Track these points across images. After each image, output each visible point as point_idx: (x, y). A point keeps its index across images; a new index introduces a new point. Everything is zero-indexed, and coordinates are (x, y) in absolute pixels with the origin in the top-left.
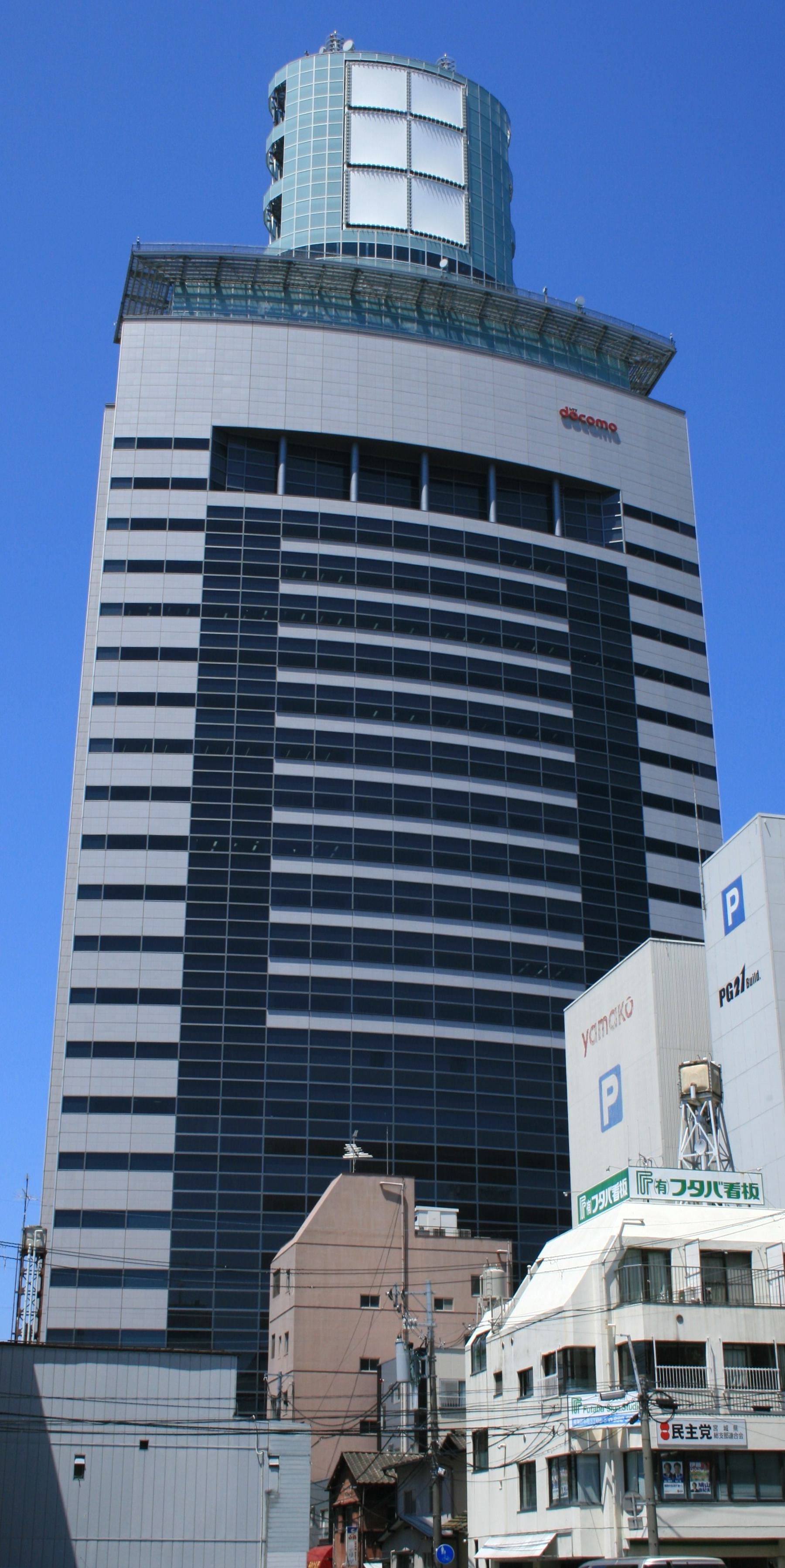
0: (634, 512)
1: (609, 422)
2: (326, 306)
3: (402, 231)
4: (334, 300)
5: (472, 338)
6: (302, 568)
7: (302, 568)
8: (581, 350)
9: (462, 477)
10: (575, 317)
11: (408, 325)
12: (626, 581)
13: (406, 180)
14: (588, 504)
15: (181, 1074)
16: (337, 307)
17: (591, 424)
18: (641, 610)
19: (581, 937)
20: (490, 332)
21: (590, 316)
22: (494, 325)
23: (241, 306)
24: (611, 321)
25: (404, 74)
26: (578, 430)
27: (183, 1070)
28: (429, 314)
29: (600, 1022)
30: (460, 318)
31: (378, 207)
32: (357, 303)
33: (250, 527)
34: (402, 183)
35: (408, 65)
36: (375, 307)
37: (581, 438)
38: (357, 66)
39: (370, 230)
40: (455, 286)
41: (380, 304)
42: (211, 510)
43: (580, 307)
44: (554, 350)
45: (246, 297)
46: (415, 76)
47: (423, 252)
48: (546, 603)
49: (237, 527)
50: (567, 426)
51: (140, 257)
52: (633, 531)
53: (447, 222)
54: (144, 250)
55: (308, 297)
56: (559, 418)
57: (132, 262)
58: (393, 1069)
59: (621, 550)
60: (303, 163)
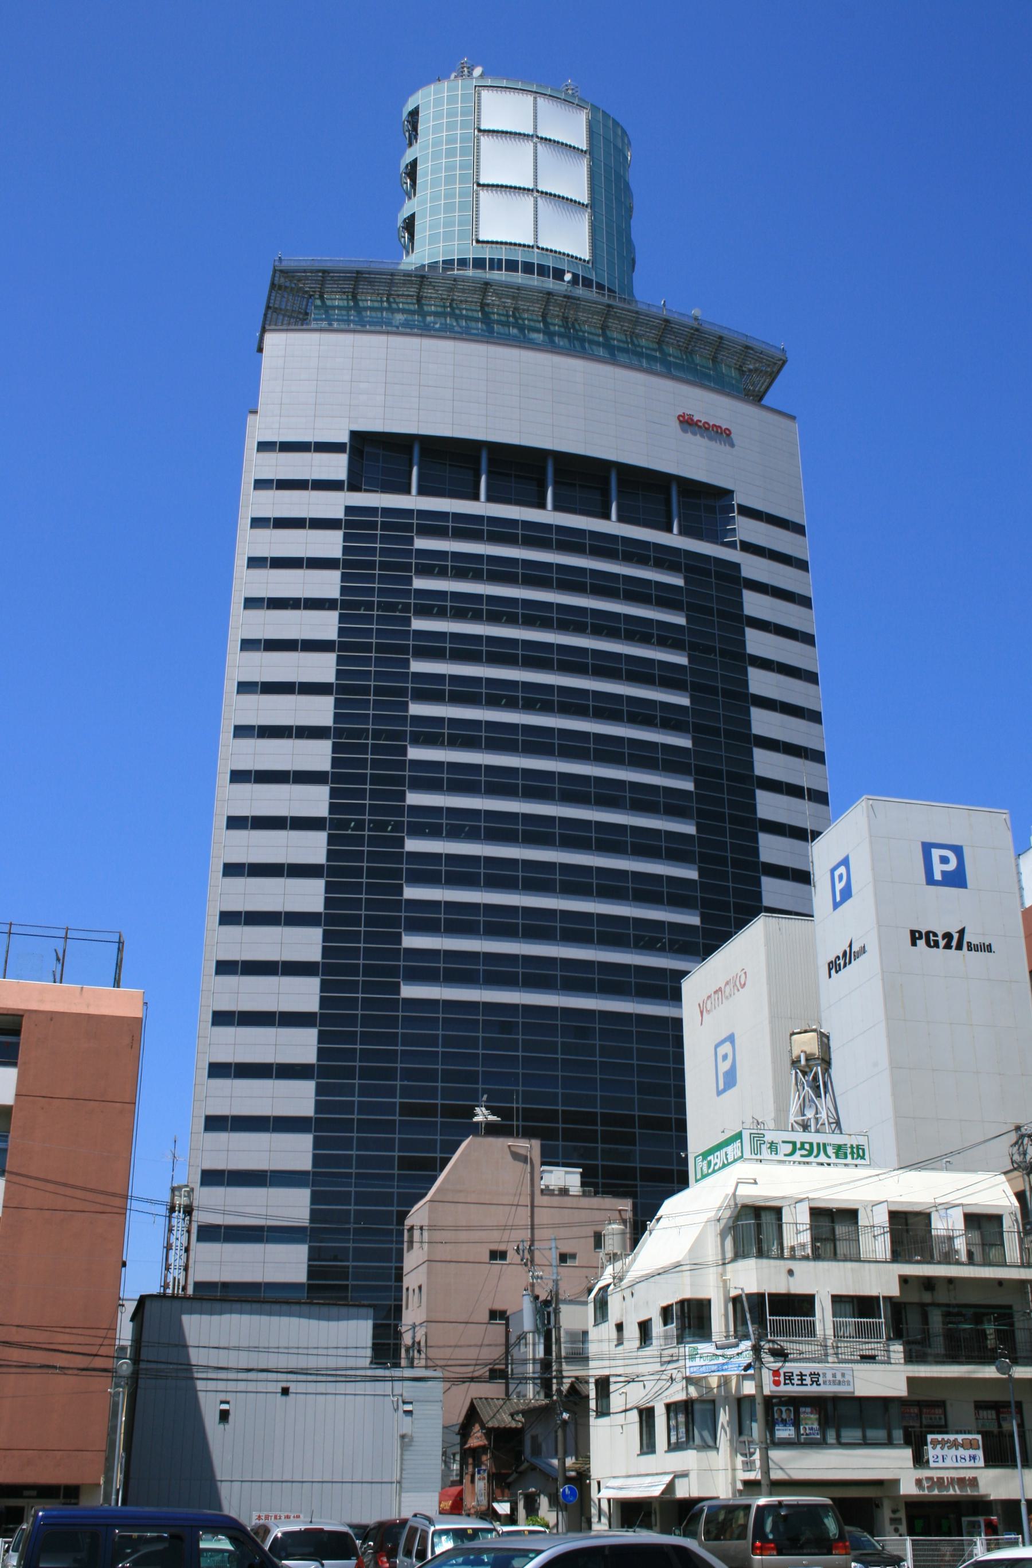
1: (724, 427)
2: (457, 318)
3: (529, 246)
4: (464, 312)
6: (435, 564)
7: (435, 564)
8: (698, 359)
9: (585, 479)
10: (692, 328)
11: (534, 336)
14: (704, 505)
17: (707, 429)
21: (706, 327)
22: (615, 335)
25: (530, 98)
26: (694, 434)
28: (555, 325)
31: (505, 224)
33: (385, 526)
34: (529, 201)
37: (698, 442)
40: (578, 299)
41: (508, 316)
42: (349, 510)
43: (696, 319)
44: (672, 359)
45: (381, 309)
46: (541, 101)
49: (373, 525)
50: (685, 431)
51: (281, 271)
52: (746, 529)
53: (572, 239)
54: (286, 265)
55: (439, 309)
57: (274, 276)
59: (735, 548)
60: (435, 183)
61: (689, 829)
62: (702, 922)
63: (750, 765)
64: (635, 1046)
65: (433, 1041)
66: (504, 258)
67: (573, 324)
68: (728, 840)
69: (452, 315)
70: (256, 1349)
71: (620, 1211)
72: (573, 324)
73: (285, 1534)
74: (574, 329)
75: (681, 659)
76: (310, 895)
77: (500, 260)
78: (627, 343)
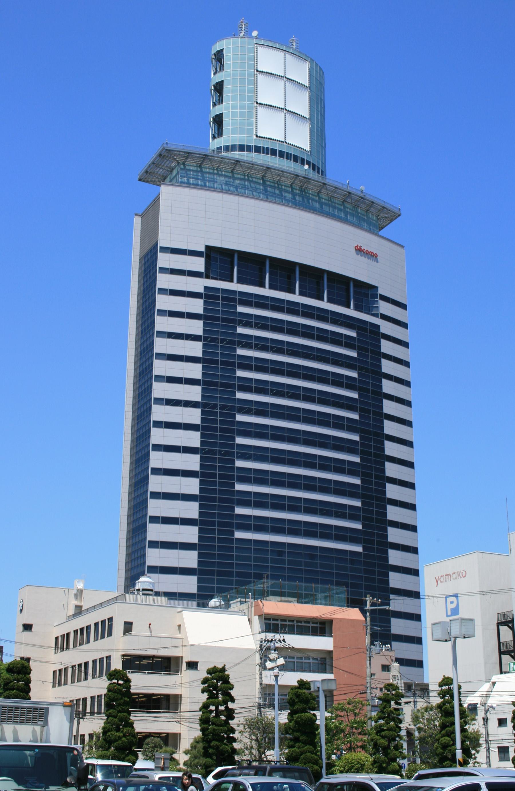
0: (384, 298)
2: (251, 182)
3: (282, 142)
4: (254, 179)
6: (249, 321)
7: (249, 321)
8: (359, 210)
9: (314, 279)
10: (360, 197)
12: (379, 332)
13: (283, 114)
14: (364, 294)
21: (367, 197)
22: (324, 197)
23: (211, 178)
24: (376, 200)
26: (361, 256)
27: (200, 555)
28: (296, 189)
29: (446, 575)
31: (270, 128)
32: (264, 181)
33: (224, 299)
34: (281, 115)
35: (284, 49)
36: (272, 184)
37: (363, 260)
41: (274, 183)
42: (206, 288)
43: (362, 192)
44: (348, 210)
45: (214, 174)
46: (287, 56)
47: (291, 154)
49: (217, 298)
50: (357, 254)
51: (167, 150)
52: (384, 308)
53: (300, 138)
54: (169, 147)
55: (242, 177)
57: (162, 150)
58: (287, 558)
59: (378, 317)
61: (357, 459)
62: (362, 505)
63: (382, 428)
65: (248, 559)
66: (270, 147)
67: (304, 189)
68: (373, 465)
69: (248, 180)
70: (460, 693)
72: (304, 189)
73: (160, 778)
74: (305, 192)
75: (354, 374)
76: (192, 486)
77: (268, 149)
78: (329, 201)
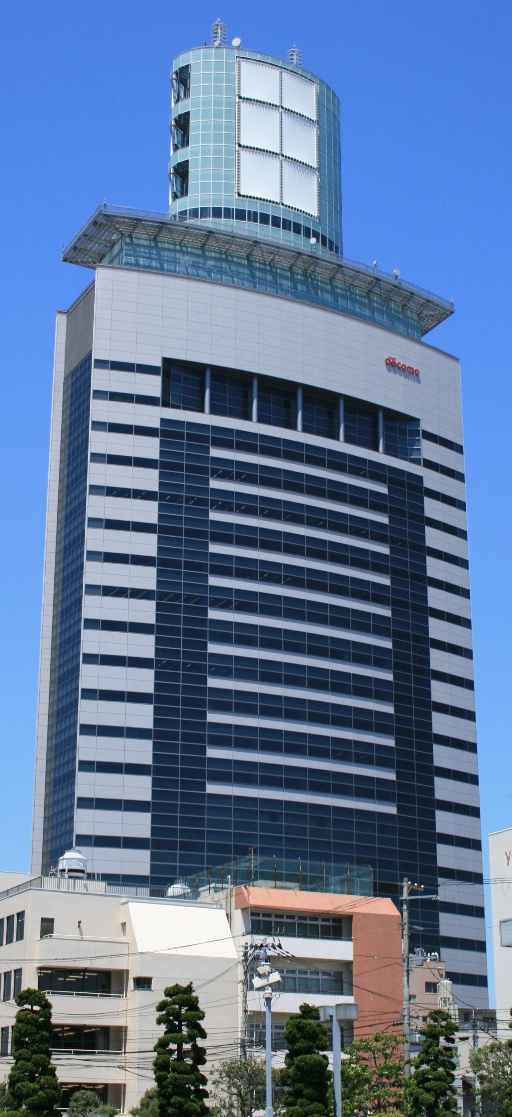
1: (415, 369)
3: (277, 203)
4: (235, 259)
5: (324, 294)
6: (228, 470)
7: (228, 470)
8: (392, 305)
9: (324, 407)
10: (393, 286)
11: (284, 282)
14: (398, 429)
15: (153, 822)
16: (238, 264)
17: (404, 370)
18: (432, 509)
19: (393, 737)
20: (336, 289)
21: (404, 285)
22: (339, 285)
23: (171, 257)
25: (276, 72)
26: (395, 373)
28: (298, 274)
30: (317, 278)
31: (257, 182)
33: (190, 437)
36: (262, 266)
37: (398, 379)
38: (245, 63)
39: (255, 200)
40: (318, 259)
41: (265, 265)
42: (163, 421)
43: (396, 277)
44: (376, 305)
45: (175, 251)
46: (285, 75)
47: (290, 222)
48: (372, 501)
50: (389, 371)
51: (105, 215)
52: (429, 450)
53: (304, 198)
54: (109, 211)
55: (217, 255)
56: (384, 365)
57: (98, 216)
58: (284, 823)
59: (419, 464)
60: (205, 138)
63: (426, 630)
64: (355, 831)
65: (227, 824)
67: (310, 274)
68: (412, 685)
69: (227, 261)
71: (439, 969)
77: (255, 213)
78: (347, 291)
